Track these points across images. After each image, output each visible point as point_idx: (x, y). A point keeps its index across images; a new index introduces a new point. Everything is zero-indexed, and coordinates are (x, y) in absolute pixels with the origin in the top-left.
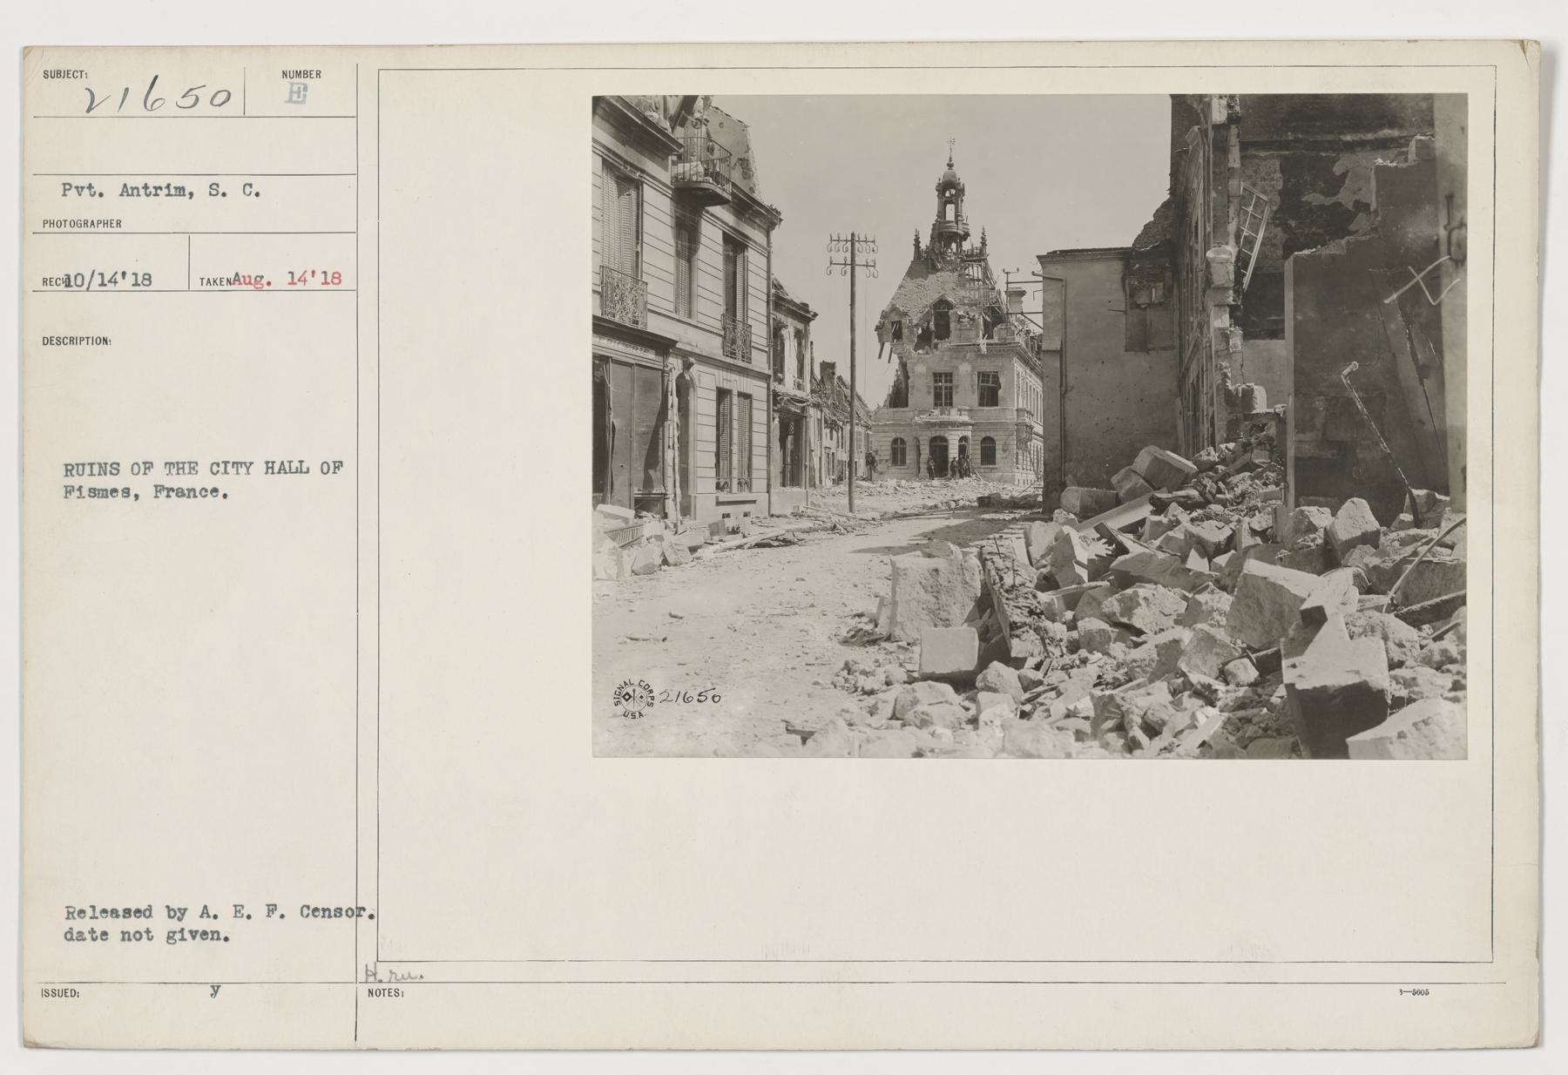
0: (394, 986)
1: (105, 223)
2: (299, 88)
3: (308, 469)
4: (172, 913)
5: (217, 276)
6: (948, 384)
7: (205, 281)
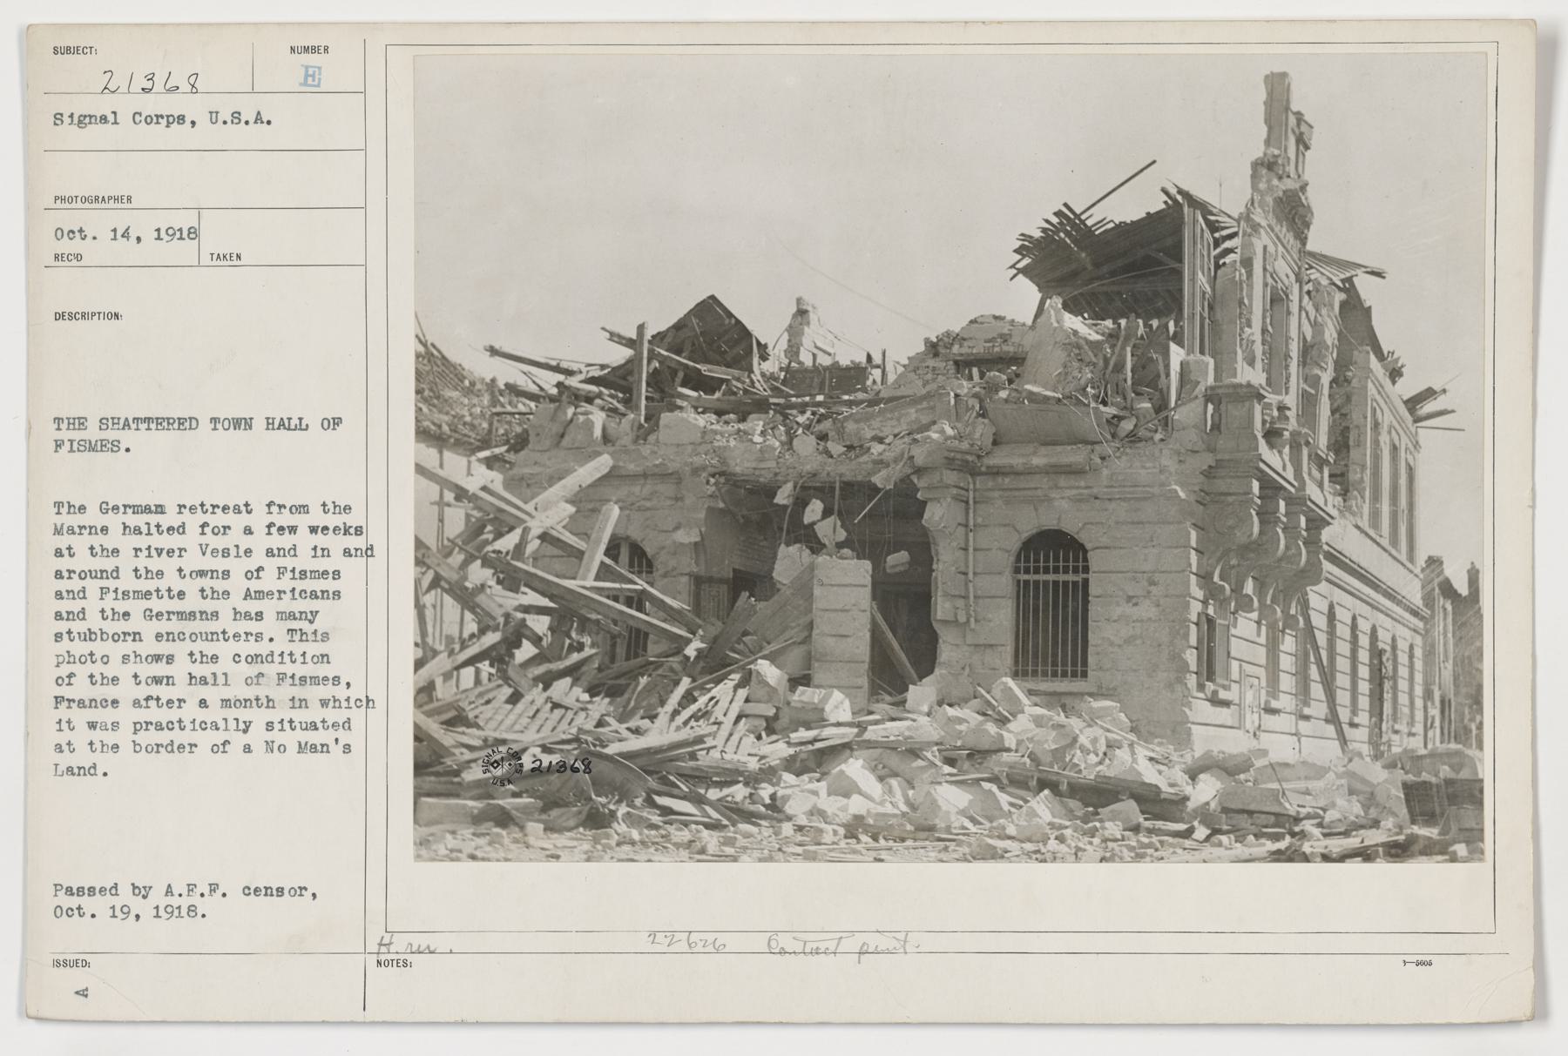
0: (402, 957)
1: (116, 199)
2: (314, 72)
3: (307, 425)
4: (137, 891)
5: (227, 251)
7: (215, 257)
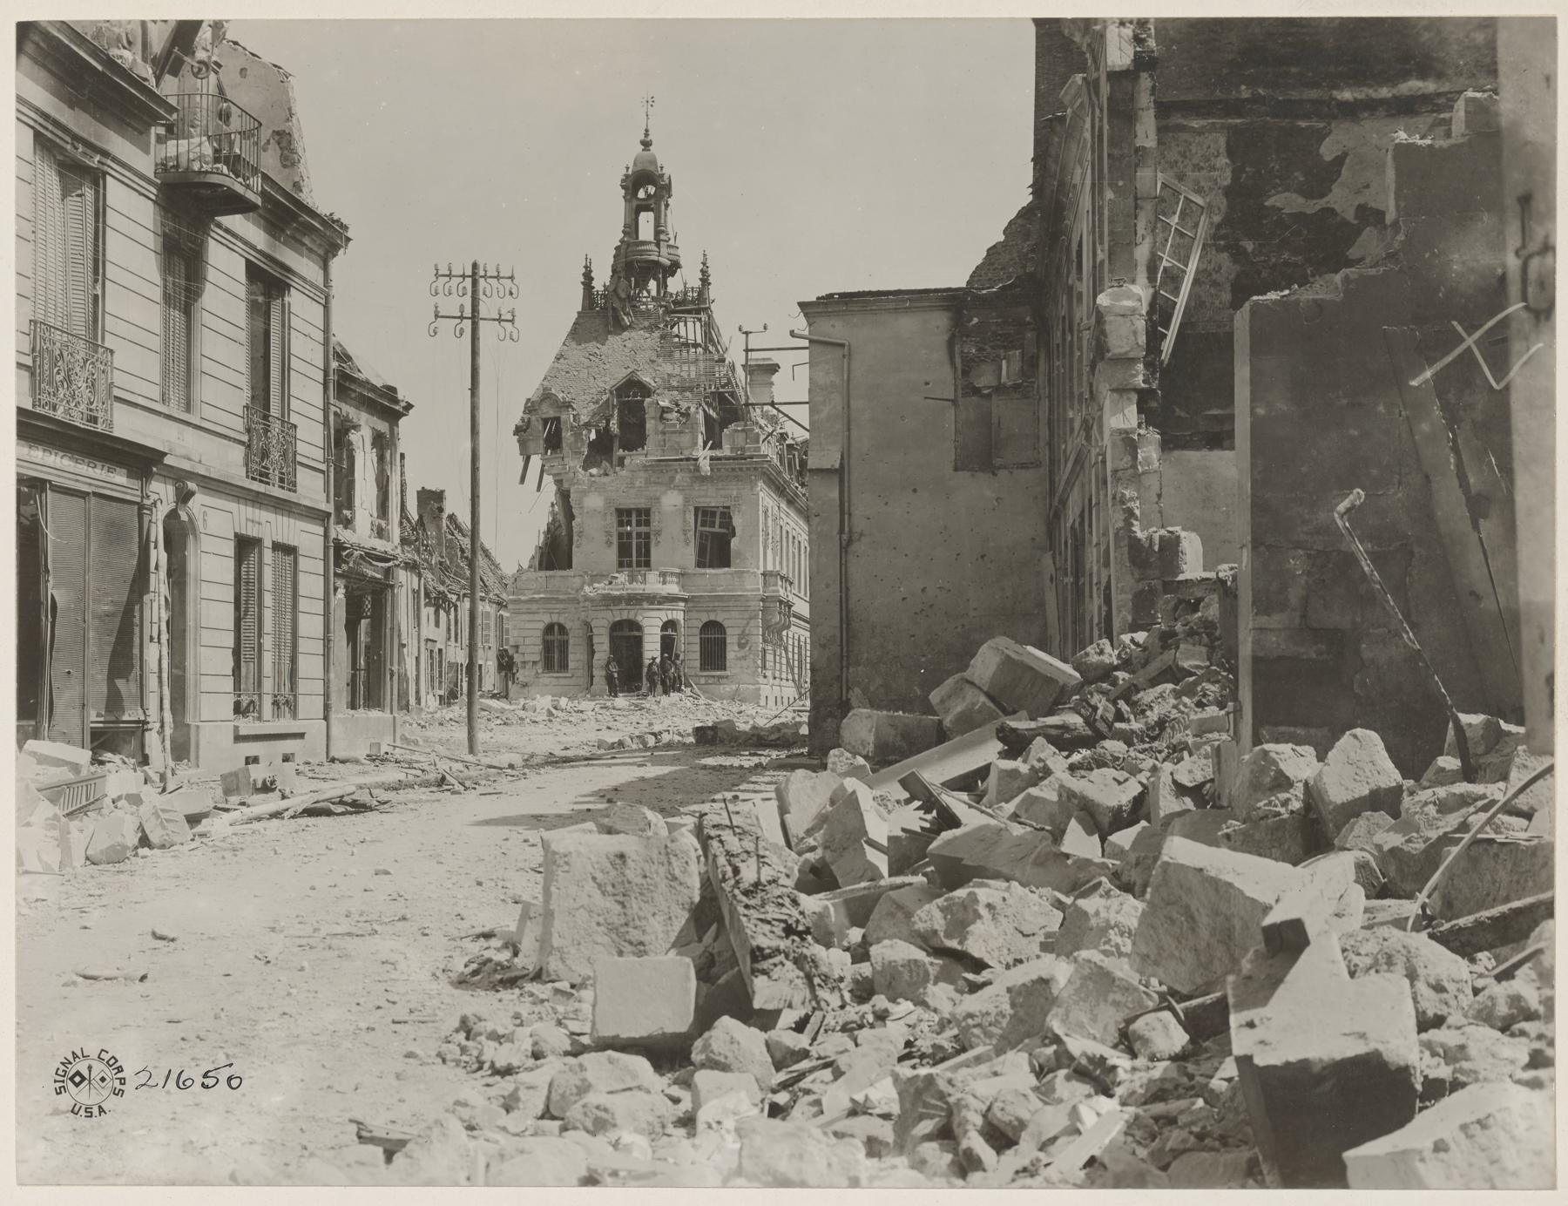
6: (643, 529)
